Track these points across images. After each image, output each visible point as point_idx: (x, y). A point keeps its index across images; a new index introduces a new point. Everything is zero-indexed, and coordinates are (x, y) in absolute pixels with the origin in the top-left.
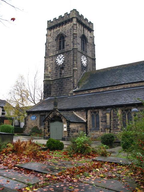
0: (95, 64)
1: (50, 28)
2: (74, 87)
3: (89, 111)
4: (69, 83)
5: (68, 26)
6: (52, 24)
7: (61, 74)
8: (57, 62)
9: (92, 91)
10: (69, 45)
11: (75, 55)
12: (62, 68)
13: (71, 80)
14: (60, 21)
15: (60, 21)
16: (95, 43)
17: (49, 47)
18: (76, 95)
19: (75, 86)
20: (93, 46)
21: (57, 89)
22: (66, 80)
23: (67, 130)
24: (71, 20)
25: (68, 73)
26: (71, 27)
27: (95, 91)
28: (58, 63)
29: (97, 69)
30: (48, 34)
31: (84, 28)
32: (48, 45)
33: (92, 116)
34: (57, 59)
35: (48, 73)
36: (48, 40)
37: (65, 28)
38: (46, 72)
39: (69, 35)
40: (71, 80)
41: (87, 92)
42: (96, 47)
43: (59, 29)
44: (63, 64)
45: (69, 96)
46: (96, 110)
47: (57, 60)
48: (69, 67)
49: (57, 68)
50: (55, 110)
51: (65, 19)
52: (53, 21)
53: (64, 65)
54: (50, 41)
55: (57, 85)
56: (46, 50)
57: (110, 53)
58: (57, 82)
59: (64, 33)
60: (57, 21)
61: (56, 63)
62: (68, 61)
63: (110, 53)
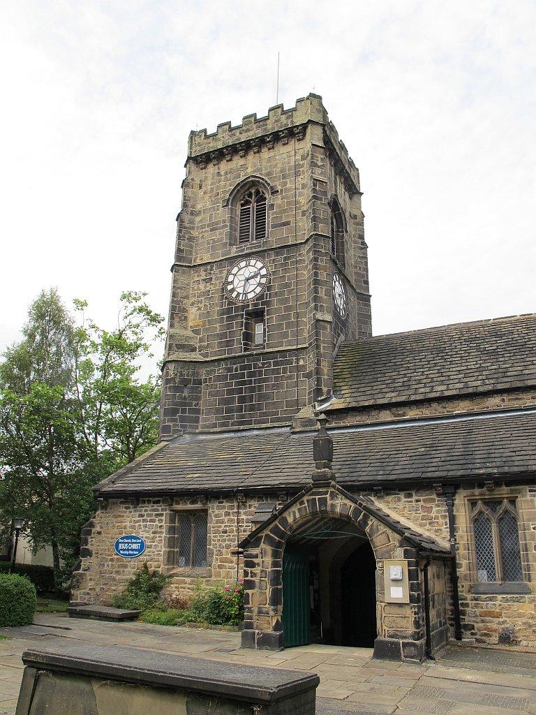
0: (369, 317)
1: (200, 160)
2: (318, 392)
3: (461, 500)
4: (290, 377)
5: (285, 154)
6: (211, 145)
7: (248, 337)
8: (233, 290)
9: (412, 413)
10: (287, 223)
11: (322, 261)
12: (257, 315)
13: (301, 363)
14: (251, 133)
15: (251, 133)
16: (367, 240)
17: (193, 228)
18: (307, 432)
19: (325, 389)
20: (362, 249)
21: (231, 401)
22: (276, 364)
23: (411, 596)
24: (295, 133)
25: (285, 335)
26: (298, 157)
27: (426, 412)
28: (234, 295)
29: (376, 332)
30: (193, 180)
31: (336, 174)
32: (191, 222)
33: (479, 524)
34: (231, 278)
35: (189, 333)
36: (189, 204)
37: (269, 160)
38: (176, 325)
39: (275, 188)
40: (301, 363)
41: (386, 416)
42: (370, 252)
43: (242, 161)
44: (260, 297)
45: (294, 433)
46: (504, 491)
47: (230, 280)
48: (288, 309)
49: (229, 311)
50: (321, 482)
51: (271, 127)
52: (214, 135)
53: (268, 303)
54: (199, 207)
55: (230, 384)
56: (180, 238)
57: (428, 271)
58: (230, 370)
59: (266, 178)
60: (237, 132)
61: (225, 292)
62: (287, 285)
63: (428, 271)
